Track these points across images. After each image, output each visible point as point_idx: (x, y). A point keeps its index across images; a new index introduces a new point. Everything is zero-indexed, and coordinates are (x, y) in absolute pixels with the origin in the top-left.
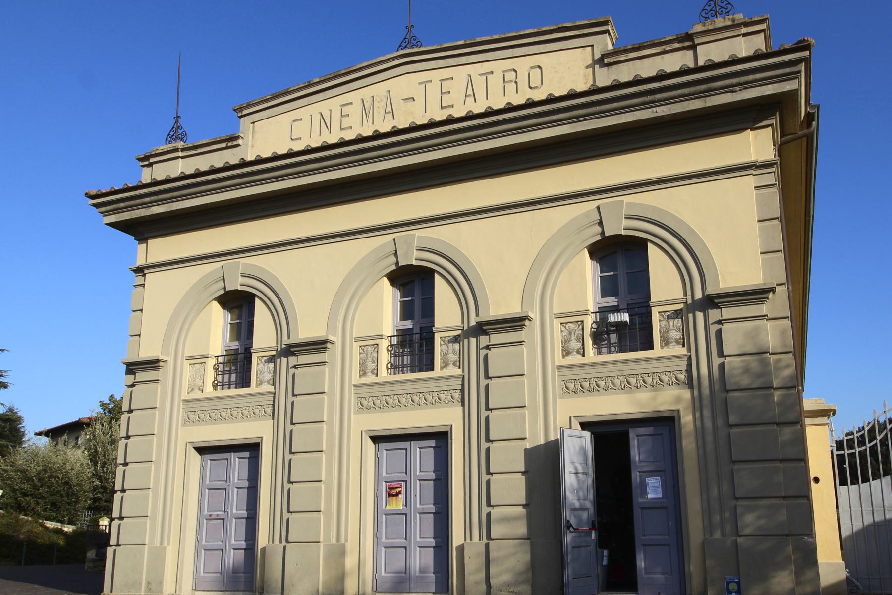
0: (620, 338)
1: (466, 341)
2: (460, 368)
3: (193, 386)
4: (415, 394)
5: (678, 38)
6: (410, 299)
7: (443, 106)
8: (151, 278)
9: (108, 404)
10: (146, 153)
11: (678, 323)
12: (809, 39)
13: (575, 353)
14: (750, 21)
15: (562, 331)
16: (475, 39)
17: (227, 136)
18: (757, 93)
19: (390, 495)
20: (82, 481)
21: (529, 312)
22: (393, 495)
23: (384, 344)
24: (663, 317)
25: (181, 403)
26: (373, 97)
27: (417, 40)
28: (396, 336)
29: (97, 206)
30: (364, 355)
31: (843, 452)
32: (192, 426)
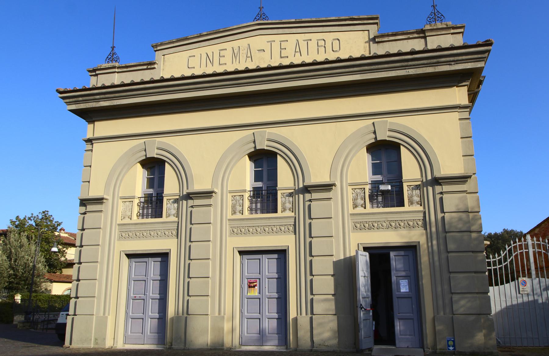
2: (293, 212)
3: (125, 215)
5: (417, 31)
6: (260, 169)
7: (282, 56)
8: (97, 146)
12: (492, 40)
13: (360, 207)
14: (455, 26)
15: (352, 193)
17: (148, 62)
18: (463, 67)
20: (2, 270)
21: (215, 189)
22: (252, 287)
23: (247, 195)
24: (409, 188)
25: (117, 226)
27: (266, 16)
28: (144, 197)
30: (234, 201)
31: (490, 268)
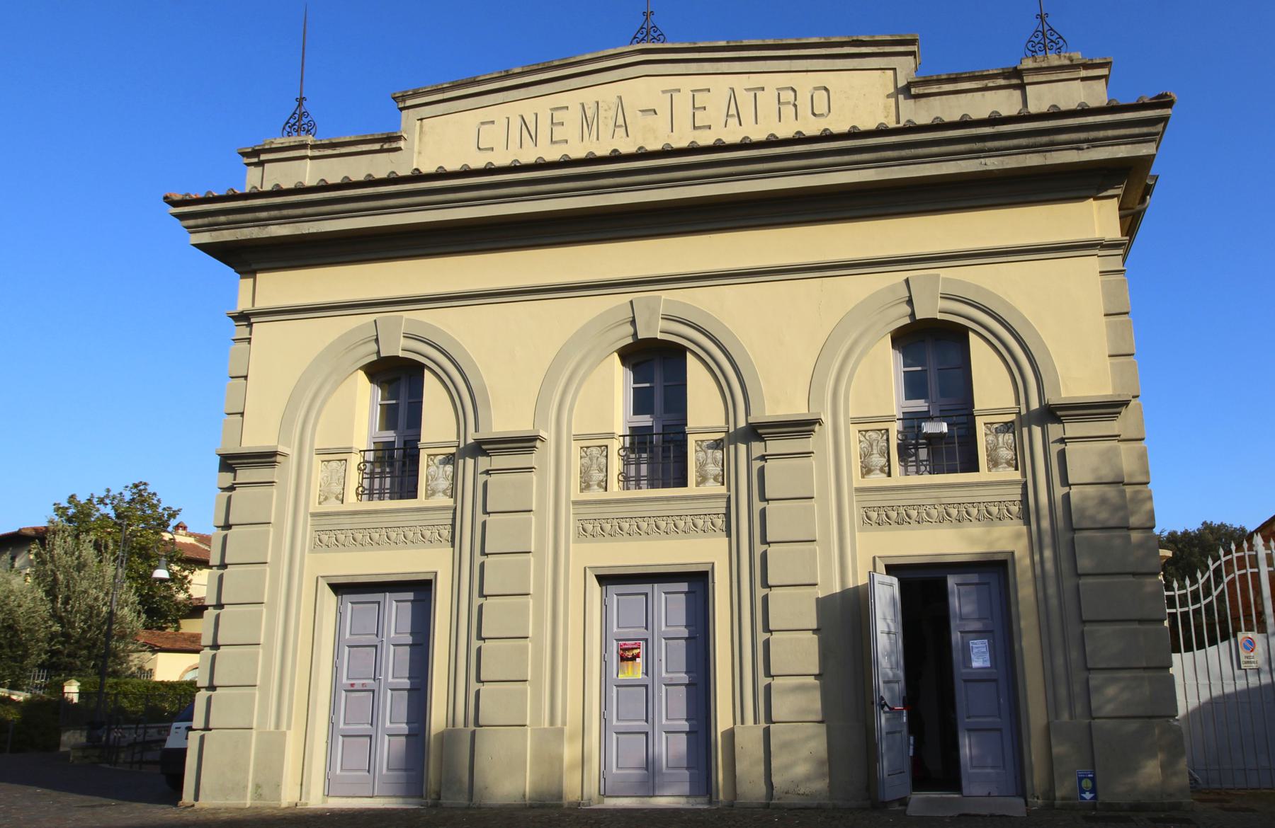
0: (933, 454)
1: (732, 447)
2: (723, 484)
4: (624, 520)
5: (1003, 73)
6: (648, 385)
7: (696, 125)
8: (261, 330)
9: (67, 508)
10: (255, 146)
11: (1009, 439)
12: (1172, 94)
13: (878, 472)
14: (1090, 62)
15: (860, 442)
16: (742, 42)
17: (382, 134)
19: (623, 659)
20: (34, 624)
22: (628, 659)
23: (616, 446)
24: (990, 429)
25: (309, 518)
26: (598, 103)
29: (181, 217)
30: (586, 460)
32: (326, 552)
